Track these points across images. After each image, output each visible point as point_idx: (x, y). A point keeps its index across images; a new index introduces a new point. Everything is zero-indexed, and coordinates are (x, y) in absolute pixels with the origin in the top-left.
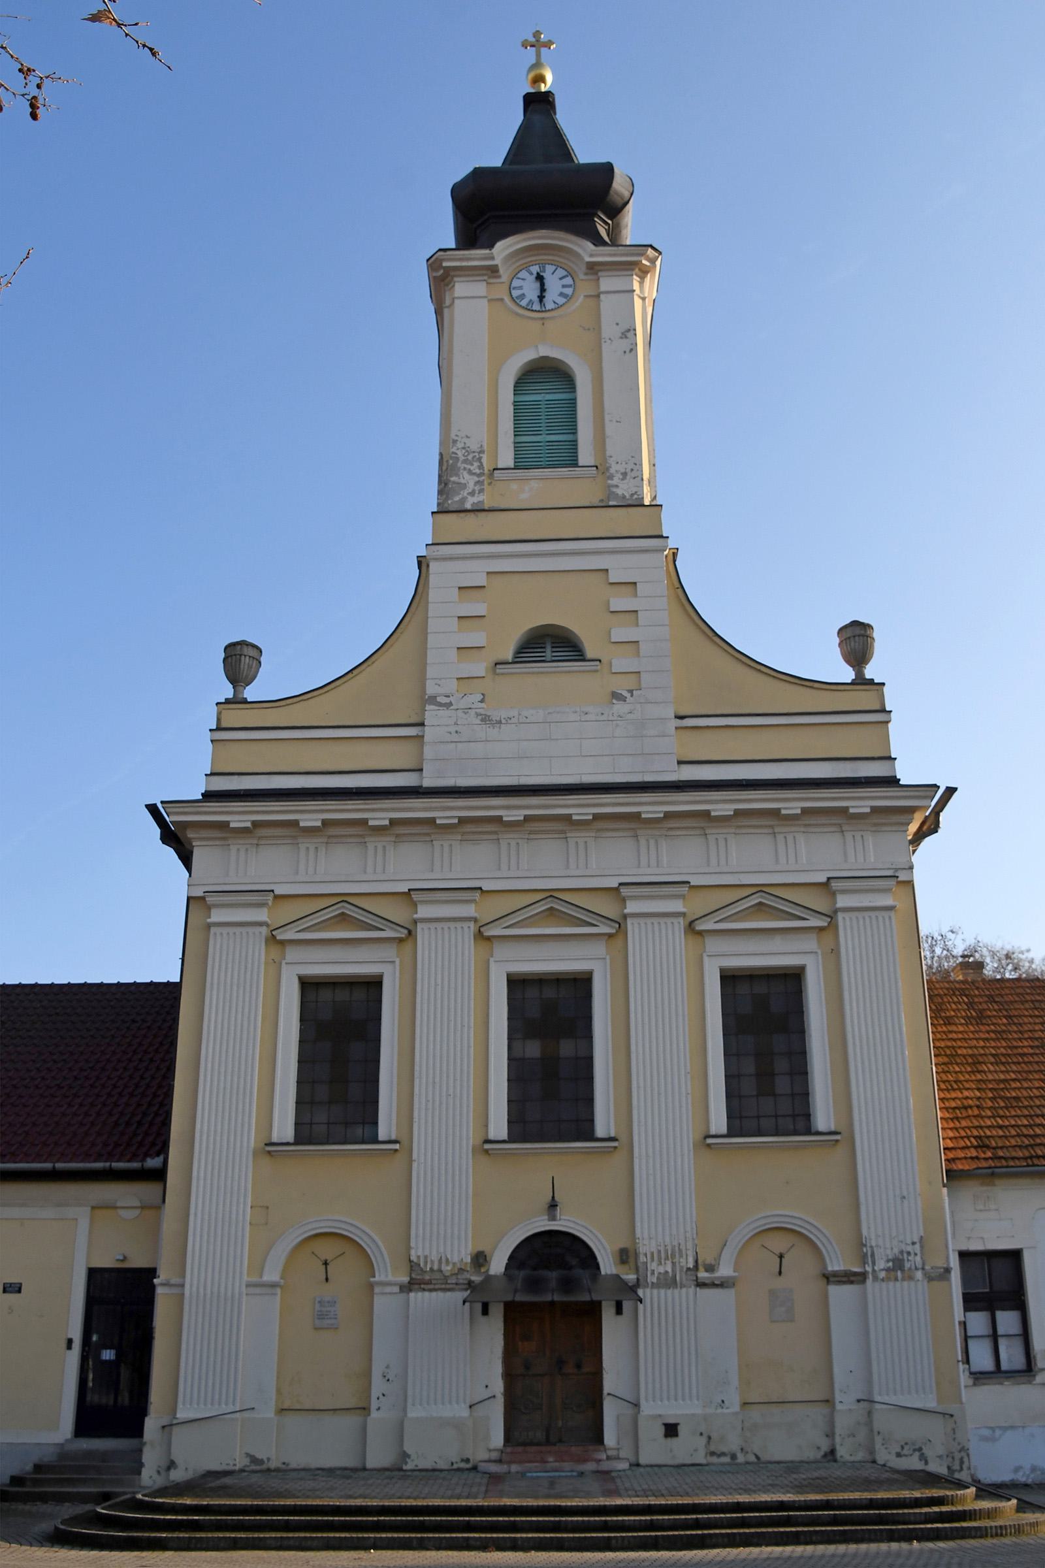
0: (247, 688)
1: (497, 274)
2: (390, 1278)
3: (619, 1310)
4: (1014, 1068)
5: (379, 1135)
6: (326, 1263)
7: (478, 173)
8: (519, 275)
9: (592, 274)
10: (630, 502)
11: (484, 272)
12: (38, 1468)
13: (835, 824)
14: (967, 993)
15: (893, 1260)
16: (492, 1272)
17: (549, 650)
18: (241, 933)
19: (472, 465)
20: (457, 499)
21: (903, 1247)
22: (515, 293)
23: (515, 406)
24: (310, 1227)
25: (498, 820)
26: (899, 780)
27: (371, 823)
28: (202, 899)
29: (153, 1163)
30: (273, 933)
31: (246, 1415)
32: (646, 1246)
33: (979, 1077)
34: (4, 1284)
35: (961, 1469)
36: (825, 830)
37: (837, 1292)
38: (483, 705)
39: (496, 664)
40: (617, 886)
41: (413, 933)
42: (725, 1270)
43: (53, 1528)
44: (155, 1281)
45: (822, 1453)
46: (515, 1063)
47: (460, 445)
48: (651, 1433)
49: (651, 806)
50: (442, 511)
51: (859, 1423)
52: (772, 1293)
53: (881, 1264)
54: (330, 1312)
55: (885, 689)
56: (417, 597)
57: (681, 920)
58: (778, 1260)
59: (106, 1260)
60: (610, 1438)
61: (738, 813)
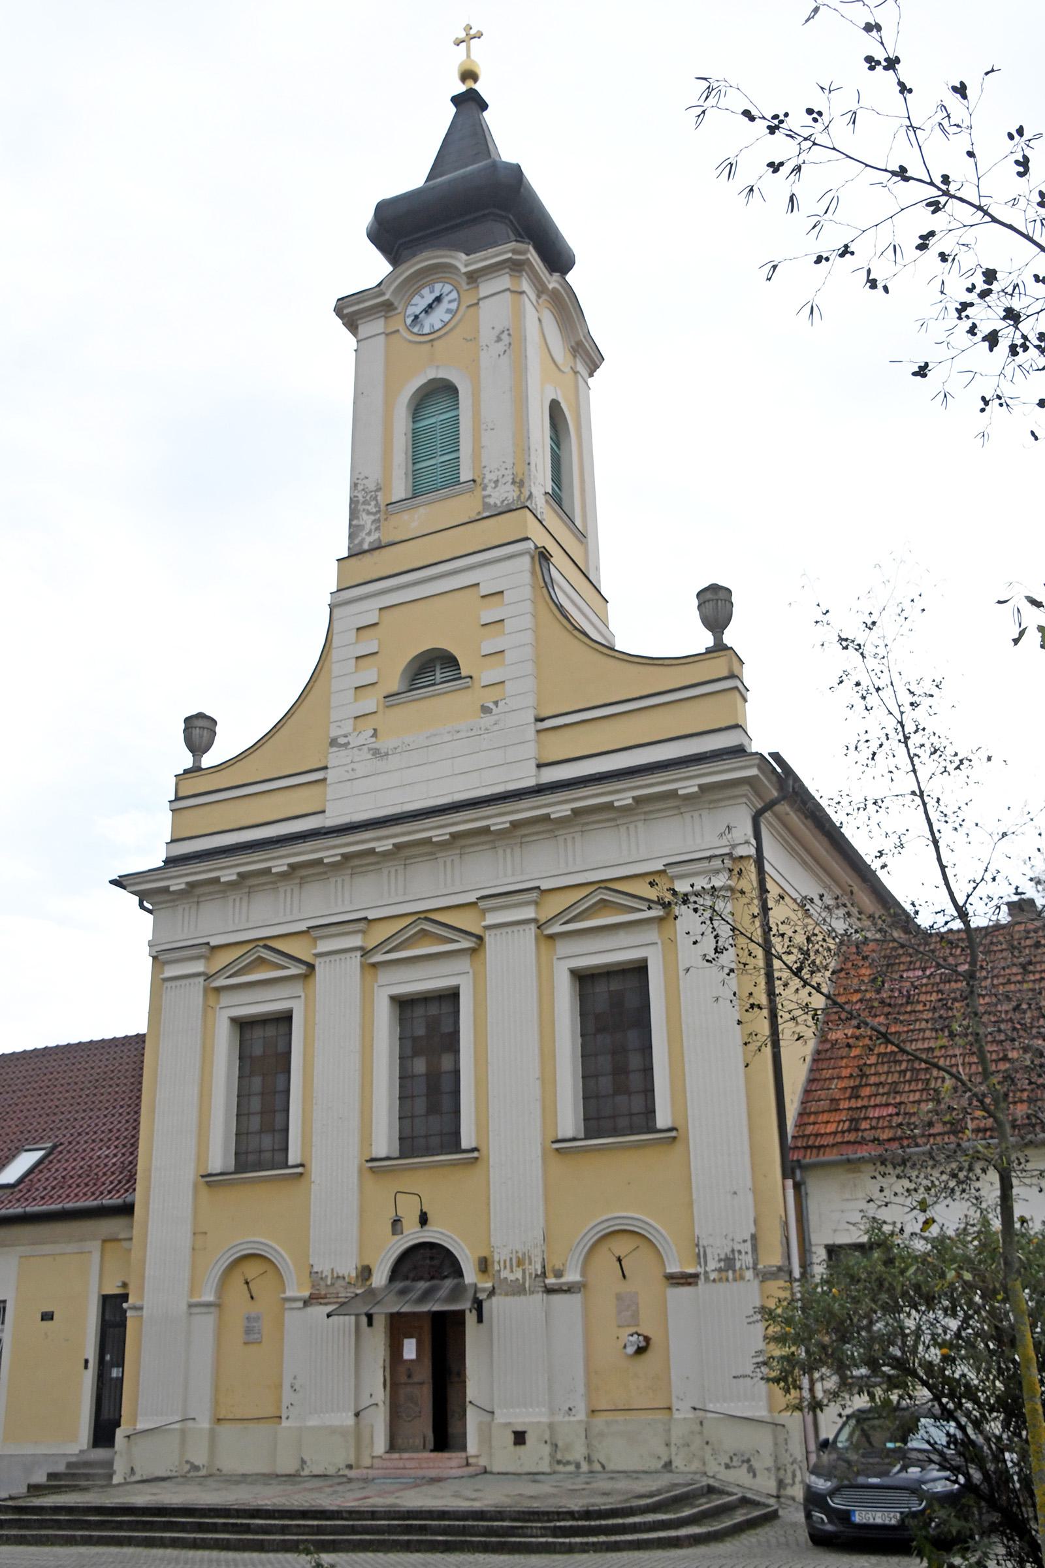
8: (413, 302)
10: (500, 510)
11: (380, 309)
19: (369, 504)
21: (737, 1247)
28: (664, 872)
32: (500, 1255)
35: (794, 1483)
36: (667, 814)
42: (572, 1276)
45: (662, 1463)
49: (498, 820)
51: (692, 1433)
52: (619, 1297)
53: (712, 1265)
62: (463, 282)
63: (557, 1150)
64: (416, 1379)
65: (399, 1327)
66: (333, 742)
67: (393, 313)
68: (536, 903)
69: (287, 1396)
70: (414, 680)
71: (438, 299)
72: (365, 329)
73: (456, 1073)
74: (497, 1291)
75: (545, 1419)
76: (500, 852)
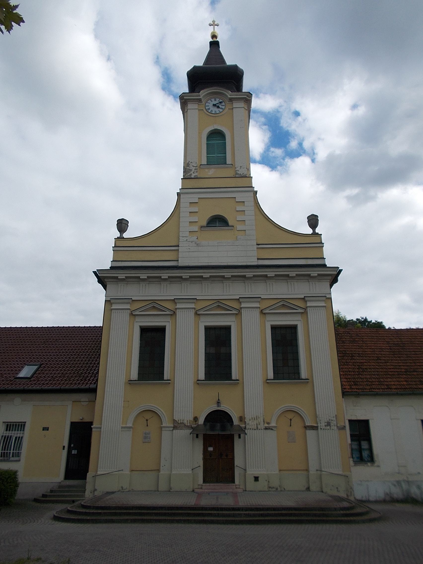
0: (124, 233)
1: (201, 101)
2: (168, 425)
3: (240, 437)
4: (365, 358)
5: (164, 378)
6: (147, 420)
7: (195, 67)
9: (230, 102)
12: (51, 491)
13: (307, 279)
14: (350, 333)
15: (327, 422)
16: (199, 424)
17: (217, 223)
18: (122, 312)
22: (207, 108)
23: (207, 144)
24: (142, 408)
25: (202, 277)
26: (327, 265)
28: (110, 301)
29: (92, 386)
30: (132, 312)
31: (120, 472)
32: (248, 416)
33: (354, 361)
34: (43, 427)
37: (310, 433)
39: (201, 227)
40: (239, 298)
41: (175, 313)
42: (273, 424)
43: (53, 515)
44: (92, 426)
46: (208, 356)
48: (250, 480)
49: (249, 273)
53: (323, 424)
54: (148, 436)
55: (322, 236)
56: (177, 206)
57: (259, 309)
58: (290, 421)
59: (76, 419)
60: (237, 481)
61: (276, 276)
63: (130, 383)
67: (201, 103)
70: (208, 224)
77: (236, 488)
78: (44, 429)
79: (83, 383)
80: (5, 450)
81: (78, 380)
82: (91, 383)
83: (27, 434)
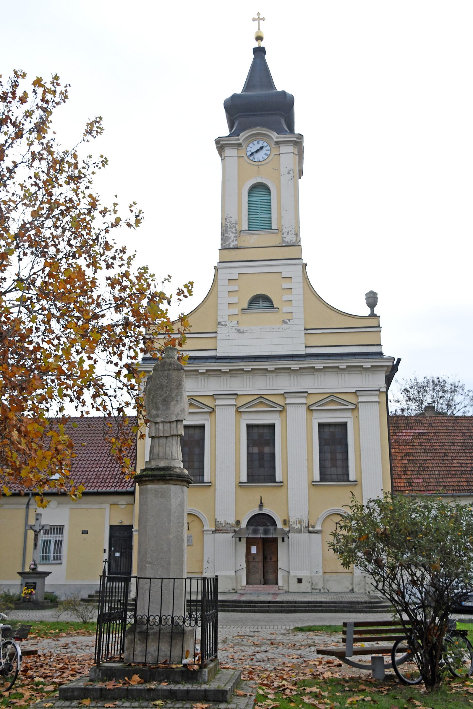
3: (283, 540)
7: (234, 97)
8: (250, 146)
10: (290, 244)
17: (261, 302)
20: (227, 243)
27: (200, 371)
32: (292, 519)
38: (237, 325)
42: (318, 528)
46: (250, 455)
47: (228, 221)
49: (295, 365)
50: (222, 249)
51: (361, 580)
62: (273, 145)
64: (256, 560)
65: (250, 542)
66: (219, 323)
68: (306, 397)
69: (205, 565)
71: (261, 148)
72: (228, 152)
73: (273, 455)
74: (291, 531)
75: (309, 575)
76: (292, 377)
77: (279, 589)
78: (83, 532)
79: (120, 486)
80: (46, 553)
81: (113, 482)
82: (128, 486)
83: (66, 537)
